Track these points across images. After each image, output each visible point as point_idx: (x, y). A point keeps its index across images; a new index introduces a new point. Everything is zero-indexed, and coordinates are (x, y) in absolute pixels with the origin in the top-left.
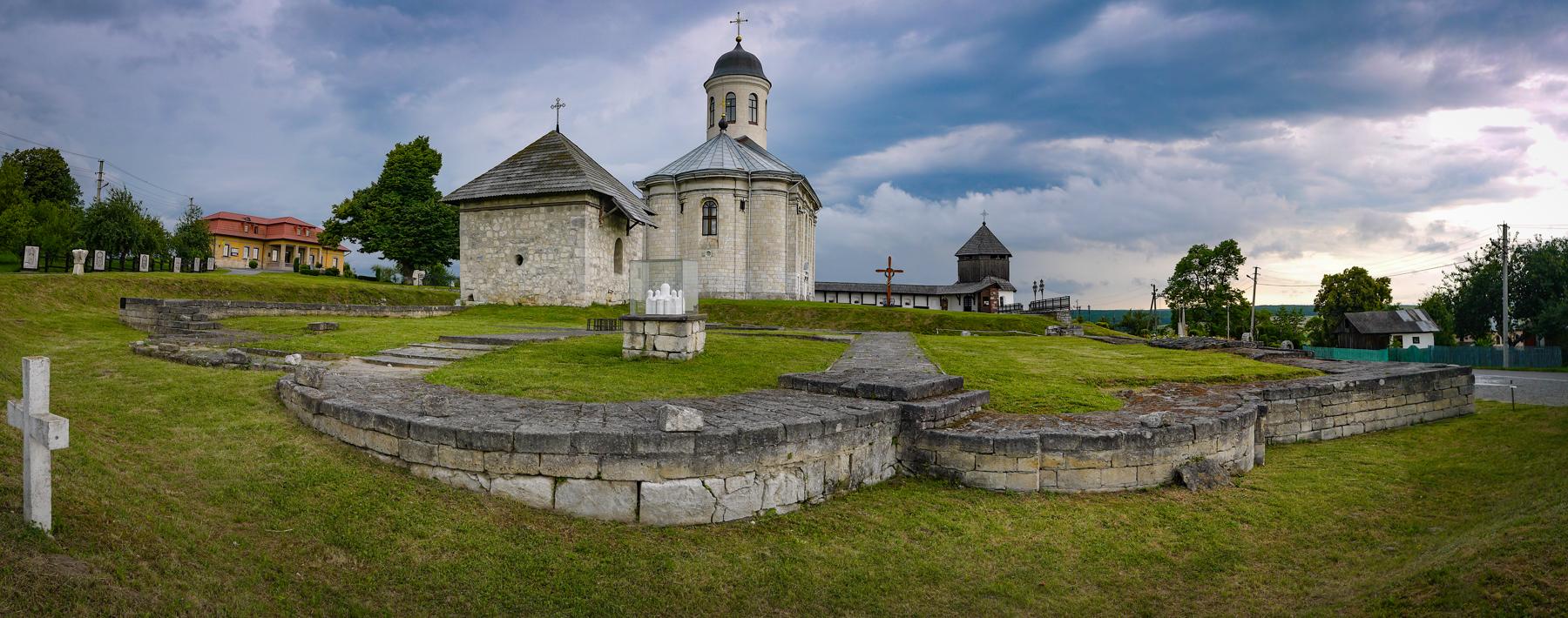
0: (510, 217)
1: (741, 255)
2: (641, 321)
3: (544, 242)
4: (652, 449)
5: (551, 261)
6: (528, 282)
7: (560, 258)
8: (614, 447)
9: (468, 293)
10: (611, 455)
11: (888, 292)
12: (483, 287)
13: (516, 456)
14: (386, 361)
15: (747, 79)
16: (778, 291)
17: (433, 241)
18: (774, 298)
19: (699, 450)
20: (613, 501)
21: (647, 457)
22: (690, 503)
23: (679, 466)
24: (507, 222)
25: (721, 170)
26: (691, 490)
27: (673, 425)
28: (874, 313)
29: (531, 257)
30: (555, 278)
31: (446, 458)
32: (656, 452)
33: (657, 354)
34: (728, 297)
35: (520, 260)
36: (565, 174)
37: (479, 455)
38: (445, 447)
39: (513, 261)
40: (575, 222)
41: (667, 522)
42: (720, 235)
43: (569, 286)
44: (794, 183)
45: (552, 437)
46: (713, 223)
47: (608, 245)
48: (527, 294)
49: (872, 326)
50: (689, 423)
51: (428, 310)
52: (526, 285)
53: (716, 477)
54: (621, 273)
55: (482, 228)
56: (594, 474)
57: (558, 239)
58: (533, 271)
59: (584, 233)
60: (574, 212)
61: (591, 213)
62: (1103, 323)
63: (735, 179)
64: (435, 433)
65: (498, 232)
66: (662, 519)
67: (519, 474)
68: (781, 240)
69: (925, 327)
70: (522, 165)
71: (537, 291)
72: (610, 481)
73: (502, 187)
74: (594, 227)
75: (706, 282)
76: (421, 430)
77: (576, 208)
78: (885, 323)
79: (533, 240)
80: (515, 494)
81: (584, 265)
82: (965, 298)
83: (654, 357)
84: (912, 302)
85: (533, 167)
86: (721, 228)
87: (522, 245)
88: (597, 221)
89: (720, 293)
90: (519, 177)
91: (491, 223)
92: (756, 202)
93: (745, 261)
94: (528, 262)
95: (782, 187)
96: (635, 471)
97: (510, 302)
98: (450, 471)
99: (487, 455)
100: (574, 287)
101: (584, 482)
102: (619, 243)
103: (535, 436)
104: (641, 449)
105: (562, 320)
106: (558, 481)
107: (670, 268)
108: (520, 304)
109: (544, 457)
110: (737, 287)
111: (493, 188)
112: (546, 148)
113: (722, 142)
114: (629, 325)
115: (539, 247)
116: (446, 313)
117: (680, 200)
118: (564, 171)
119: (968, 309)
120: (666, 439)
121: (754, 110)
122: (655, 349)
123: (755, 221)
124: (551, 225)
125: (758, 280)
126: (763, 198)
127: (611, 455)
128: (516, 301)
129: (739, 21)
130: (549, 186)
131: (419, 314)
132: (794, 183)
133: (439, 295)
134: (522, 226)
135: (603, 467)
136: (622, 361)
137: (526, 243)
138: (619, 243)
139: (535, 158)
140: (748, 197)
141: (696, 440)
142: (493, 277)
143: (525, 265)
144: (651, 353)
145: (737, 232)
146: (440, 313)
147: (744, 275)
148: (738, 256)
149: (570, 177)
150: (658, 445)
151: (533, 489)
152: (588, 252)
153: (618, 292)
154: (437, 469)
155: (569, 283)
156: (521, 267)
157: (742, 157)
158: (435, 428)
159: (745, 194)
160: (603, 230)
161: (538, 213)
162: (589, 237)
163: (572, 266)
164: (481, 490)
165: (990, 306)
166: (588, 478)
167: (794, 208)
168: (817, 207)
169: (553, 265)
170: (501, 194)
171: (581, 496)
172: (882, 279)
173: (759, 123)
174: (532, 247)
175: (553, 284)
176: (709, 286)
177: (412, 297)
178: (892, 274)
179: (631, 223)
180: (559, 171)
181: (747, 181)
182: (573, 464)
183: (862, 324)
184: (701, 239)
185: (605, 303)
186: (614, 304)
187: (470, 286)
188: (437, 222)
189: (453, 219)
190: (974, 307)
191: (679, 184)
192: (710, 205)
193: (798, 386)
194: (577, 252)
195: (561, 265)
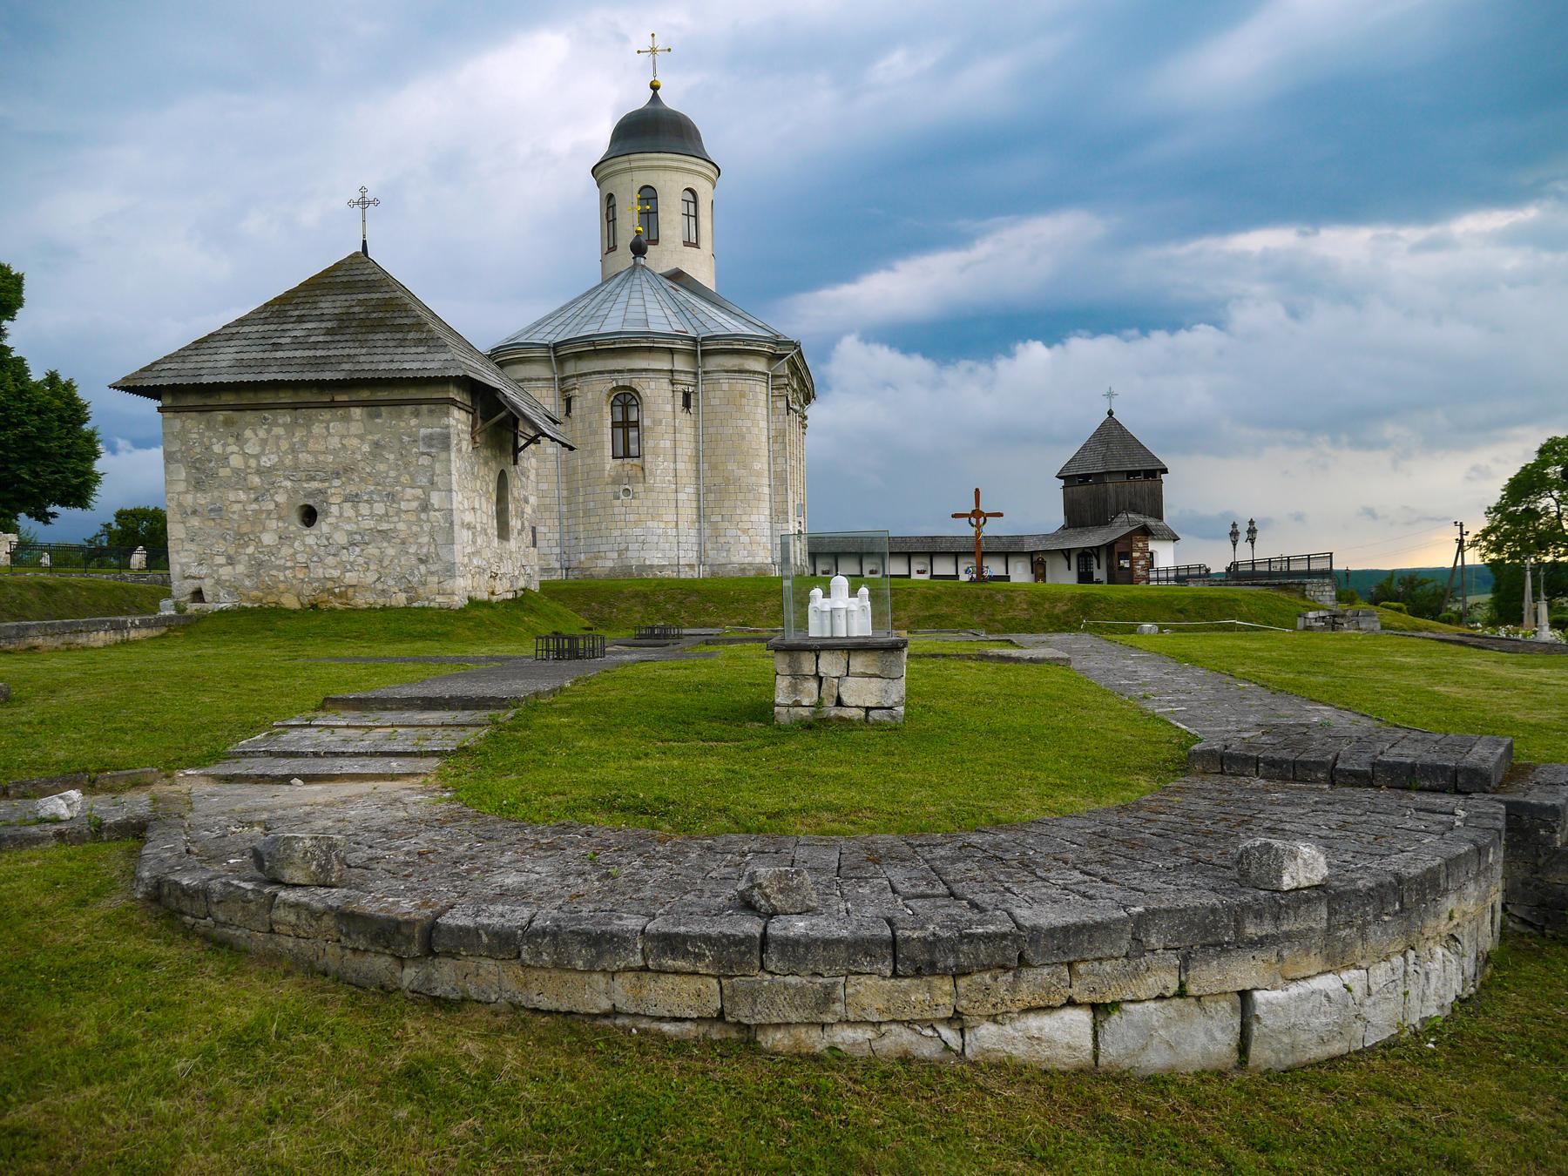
0: (284, 425)
1: (687, 494)
2: (810, 651)
3: (362, 480)
4: (1268, 928)
5: (381, 518)
6: (330, 560)
7: (399, 512)
8: (1206, 931)
9: (190, 586)
10: (1203, 946)
11: (979, 550)
12: (226, 572)
13: (1028, 975)
14: (286, 771)
15: (680, 161)
16: (758, 560)
17: (13, 466)
18: (752, 573)
19: (1334, 921)
20: (1202, 1035)
21: (1260, 943)
22: (1324, 1020)
23: (1307, 951)
24: (278, 437)
25: (648, 335)
26: (1327, 996)
27: (1293, 878)
28: (955, 594)
29: (334, 510)
30: (391, 552)
31: (865, 1001)
32: (1274, 931)
33: (846, 713)
34: (667, 573)
35: (309, 516)
36: (402, 343)
37: (946, 985)
38: (863, 979)
39: (295, 518)
40: (429, 440)
41: (1289, 1061)
42: (648, 458)
43: (423, 568)
44: (782, 357)
45: (1098, 926)
46: (633, 434)
47: (487, 484)
48: (329, 585)
49: (959, 619)
50: (1312, 870)
51: (119, 627)
52: (325, 567)
53: (1356, 968)
54: (508, 540)
55: (217, 449)
56: (1174, 987)
57: (392, 474)
58: (341, 538)
59: (449, 460)
60: (426, 420)
61: (458, 421)
62: (1395, 604)
63: (671, 351)
64: (841, 953)
65: (257, 457)
66: (1282, 1056)
67: (1029, 1010)
68: (761, 464)
69: (1058, 618)
70: (301, 319)
71: (351, 578)
72: (1198, 998)
73: (263, 364)
74: (464, 449)
75: (623, 546)
76: (801, 950)
77: (431, 411)
78: (981, 613)
79: (337, 475)
80: (1020, 1051)
81: (452, 524)
82: (1079, 556)
83: (841, 719)
84: (881, 569)
85: (329, 325)
86: (649, 444)
87: (315, 485)
88: (468, 437)
89: (651, 566)
90: (297, 343)
91: (239, 438)
92: (711, 394)
93: (694, 504)
94: (329, 520)
95: (759, 365)
96: (1243, 972)
97: (290, 602)
98: (870, 1028)
99: (963, 983)
100: (433, 568)
101: (1152, 1005)
102: (502, 482)
103: (1066, 929)
104: (1251, 930)
105: (422, 637)
106: (1100, 1010)
107: (549, 522)
108: (314, 606)
109: (1081, 967)
110: (682, 554)
111: (240, 364)
112: (349, 287)
113: (639, 280)
114: (787, 659)
115: (352, 489)
116: (155, 632)
117: (563, 391)
118: (399, 336)
119: (1085, 577)
120: (1287, 906)
121: (692, 220)
122: (839, 702)
123: (712, 430)
124: (376, 444)
125: (722, 540)
126: (725, 387)
127: (1203, 946)
128: (305, 601)
129: (653, 51)
130: (373, 367)
131: (100, 638)
132: (782, 357)
133: (88, 589)
134: (312, 445)
135: (1191, 973)
136: (785, 732)
137: (322, 481)
138: (502, 482)
139: (329, 305)
140: (696, 386)
141: (1329, 903)
142: (250, 550)
143: (323, 526)
144: (834, 712)
145: (679, 451)
146: (144, 632)
147: (693, 532)
148: (682, 496)
149: (413, 350)
150: (1276, 918)
151: (1058, 1035)
152: (457, 498)
153: (505, 574)
154: (837, 1029)
155: (421, 561)
156: (314, 530)
157: (681, 310)
158: (839, 941)
159: (689, 379)
160: (478, 455)
161: (347, 419)
162: (458, 470)
163: (426, 527)
164: (946, 1055)
165: (1131, 569)
166: (1161, 998)
167: (782, 404)
168: (809, 397)
169: (385, 526)
170: (265, 377)
171: (1148, 1032)
172: (964, 529)
173: (701, 245)
174: (336, 490)
175: (386, 563)
176: (629, 554)
177: (29, 595)
178: (982, 520)
179: (522, 442)
180: (388, 335)
181: (693, 354)
182: (1136, 973)
183: (938, 616)
184: (610, 464)
185: (486, 597)
186: (501, 597)
187: (194, 571)
188: (22, 423)
189: (61, 419)
190: (1100, 573)
191: (561, 361)
192: (626, 399)
193: (1235, 769)
194: (436, 499)
195: (401, 526)
